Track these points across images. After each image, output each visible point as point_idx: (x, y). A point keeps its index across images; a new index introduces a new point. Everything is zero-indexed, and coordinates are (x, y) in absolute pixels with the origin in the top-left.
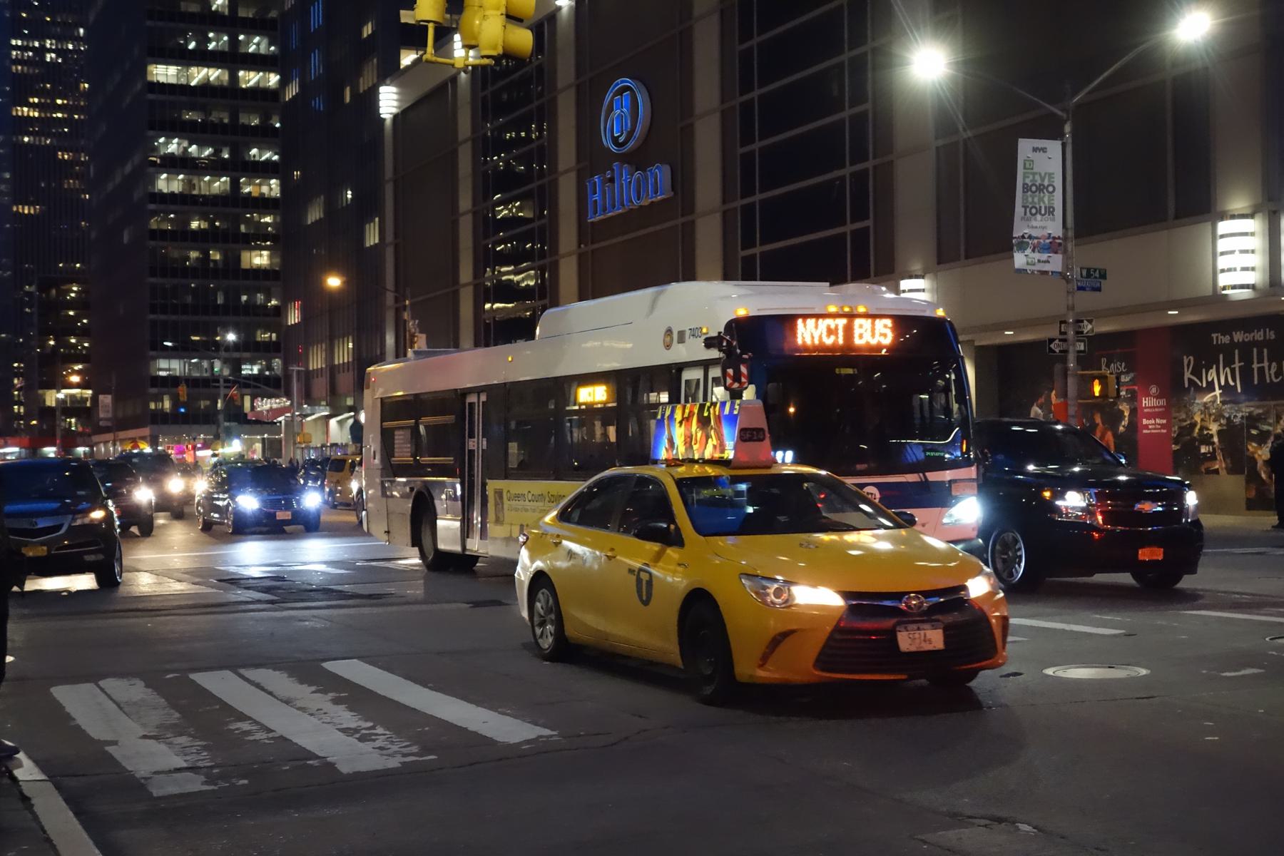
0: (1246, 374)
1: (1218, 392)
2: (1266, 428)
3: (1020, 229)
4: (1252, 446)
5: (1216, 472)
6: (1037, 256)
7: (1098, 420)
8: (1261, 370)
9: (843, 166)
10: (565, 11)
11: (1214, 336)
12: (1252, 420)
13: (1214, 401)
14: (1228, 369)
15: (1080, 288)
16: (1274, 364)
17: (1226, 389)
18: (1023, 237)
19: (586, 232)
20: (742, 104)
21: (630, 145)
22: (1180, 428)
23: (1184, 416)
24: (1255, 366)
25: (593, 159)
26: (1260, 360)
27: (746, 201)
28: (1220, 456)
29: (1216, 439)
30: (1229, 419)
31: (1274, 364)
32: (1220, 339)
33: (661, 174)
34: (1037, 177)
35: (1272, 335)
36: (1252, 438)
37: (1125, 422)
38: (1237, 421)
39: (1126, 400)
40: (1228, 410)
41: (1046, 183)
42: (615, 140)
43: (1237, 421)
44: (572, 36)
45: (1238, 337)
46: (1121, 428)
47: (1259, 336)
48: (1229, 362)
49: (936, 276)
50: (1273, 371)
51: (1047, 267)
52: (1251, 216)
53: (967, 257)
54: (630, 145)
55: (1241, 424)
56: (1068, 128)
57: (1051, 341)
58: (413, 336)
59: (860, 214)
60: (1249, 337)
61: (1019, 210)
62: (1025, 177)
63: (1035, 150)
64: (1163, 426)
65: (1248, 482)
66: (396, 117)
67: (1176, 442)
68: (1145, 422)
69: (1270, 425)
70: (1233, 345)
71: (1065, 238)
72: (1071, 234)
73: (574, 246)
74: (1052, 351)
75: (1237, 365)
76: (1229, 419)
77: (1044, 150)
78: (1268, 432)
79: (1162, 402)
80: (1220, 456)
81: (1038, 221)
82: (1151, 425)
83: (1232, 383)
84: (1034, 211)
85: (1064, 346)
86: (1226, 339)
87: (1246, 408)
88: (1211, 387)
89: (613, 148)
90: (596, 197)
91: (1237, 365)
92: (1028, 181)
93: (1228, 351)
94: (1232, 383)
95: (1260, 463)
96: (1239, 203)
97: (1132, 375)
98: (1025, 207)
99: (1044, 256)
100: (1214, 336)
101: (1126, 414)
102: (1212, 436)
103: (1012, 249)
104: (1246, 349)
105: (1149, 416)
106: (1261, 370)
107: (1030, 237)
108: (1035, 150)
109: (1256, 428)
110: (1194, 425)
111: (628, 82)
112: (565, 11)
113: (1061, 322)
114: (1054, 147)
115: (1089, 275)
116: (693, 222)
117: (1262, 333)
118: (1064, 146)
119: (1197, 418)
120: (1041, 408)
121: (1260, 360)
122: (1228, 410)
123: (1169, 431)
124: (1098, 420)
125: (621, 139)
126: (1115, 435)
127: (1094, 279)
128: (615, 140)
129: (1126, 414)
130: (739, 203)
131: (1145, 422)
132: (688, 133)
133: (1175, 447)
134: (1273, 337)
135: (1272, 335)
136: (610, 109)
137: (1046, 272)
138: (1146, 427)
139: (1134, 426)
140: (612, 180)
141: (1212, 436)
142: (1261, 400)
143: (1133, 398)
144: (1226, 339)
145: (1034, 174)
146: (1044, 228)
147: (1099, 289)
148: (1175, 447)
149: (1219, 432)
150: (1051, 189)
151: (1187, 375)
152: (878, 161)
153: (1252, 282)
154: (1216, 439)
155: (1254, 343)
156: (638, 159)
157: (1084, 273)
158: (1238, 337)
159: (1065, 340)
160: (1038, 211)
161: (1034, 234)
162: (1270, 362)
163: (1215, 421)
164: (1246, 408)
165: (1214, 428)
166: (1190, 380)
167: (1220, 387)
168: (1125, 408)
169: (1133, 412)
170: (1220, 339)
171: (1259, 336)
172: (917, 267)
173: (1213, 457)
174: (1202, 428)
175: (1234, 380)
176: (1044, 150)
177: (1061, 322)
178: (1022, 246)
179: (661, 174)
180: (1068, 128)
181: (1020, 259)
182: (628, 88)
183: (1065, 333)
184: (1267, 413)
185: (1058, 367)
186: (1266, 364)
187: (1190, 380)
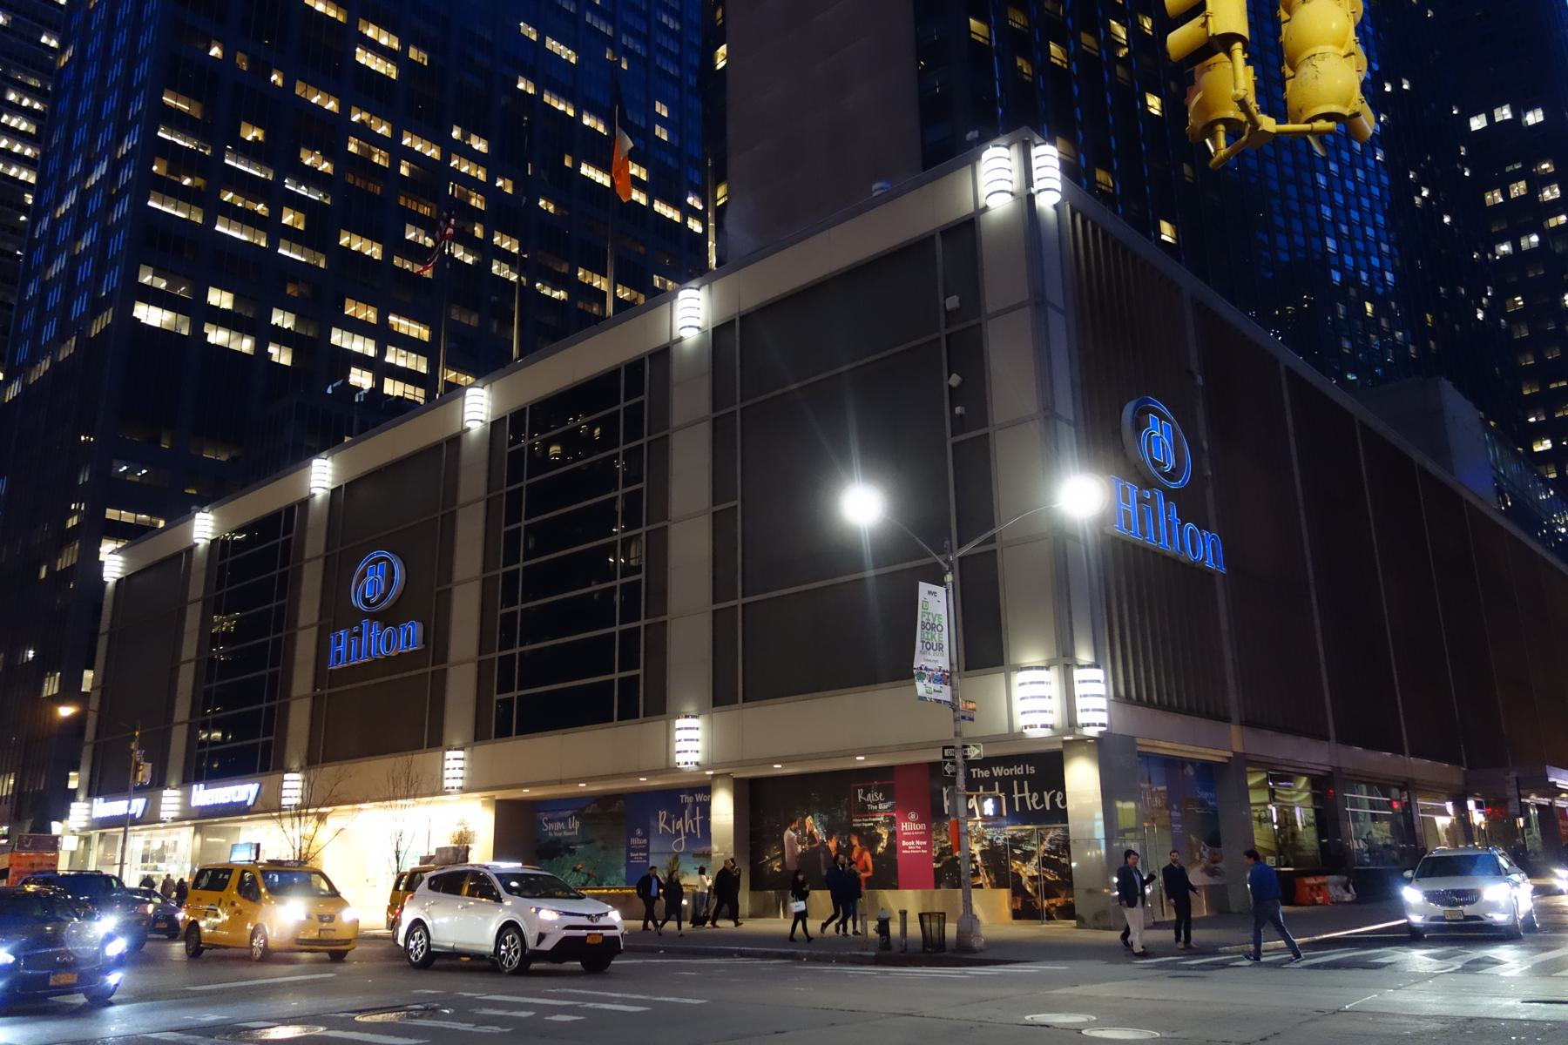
2: (1029, 848)
4: (1016, 865)
5: (980, 886)
6: (933, 686)
7: (855, 841)
8: (1022, 800)
10: (201, 547)
12: (1015, 841)
17: (689, 835)
19: (322, 676)
20: (505, 575)
21: (384, 605)
24: (1016, 796)
25: (337, 613)
26: (1021, 790)
27: (633, 625)
28: (983, 872)
29: (978, 858)
33: (415, 629)
36: (1016, 857)
37: (884, 844)
38: (1000, 842)
39: (884, 825)
40: (990, 833)
42: (366, 602)
43: (1000, 842)
44: (484, 455)
45: (998, 771)
46: (880, 849)
47: (1019, 771)
49: (711, 719)
51: (940, 697)
52: (1047, 668)
53: (744, 701)
54: (384, 605)
58: (138, 764)
59: (268, 732)
60: (1009, 772)
61: (918, 644)
64: (923, 847)
65: (1014, 895)
66: (119, 581)
67: (937, 860)
70: (992, 778)
73: (308, 689)
77: (934, 593)
78: (1033, 852)
79: (922, 826)
80: (983, 872)
81: (931, 655)
82: (910, 847)
86: (986, 774)
87: (1011, 830)
89: (364, 608)
90: (340, 648)
95: (1025, 879)
96: (1032, 657)
97: (889, 804)
99: (938, 687)
105: (908, 839)
106: (1022, 800)
111: (385, 554)
112: (201, 547)
114: (941, 590)
116: (445, 670)
121: (1021, 790)
122: (990, 833)
123: (930, 852)
124: (855, 841)
125: (373, 600)
126: (873, 856)
128: (366, 602)
132: (445, 599)
133: (935, 865)
136: (364, 575)
137: (939, 701)
138: (906, 848)
139: (892, 847)
140: (359, 634)
143: (892, 822)
144: (986, 774)
148: (935, 865)
149: (982, 853)
152: (746, 600)
153: (1049, 722)
154: (978, 858)
155: (1014, 777)
156: (390, 617)
158: (998, 771)
162: (1031, 792)
164: (1011, 830)
165: (976, 849)
168: (884, 833)
169: (892, 835)
171: (1019, 771)
172: (691, 709)
173: (976, 874)
176: (934, 593)
178: (921, 677)
179: (415, 629)
180: (949, 578)
181: (922, 688)
182: (383, 559)
186: (1027, 794)
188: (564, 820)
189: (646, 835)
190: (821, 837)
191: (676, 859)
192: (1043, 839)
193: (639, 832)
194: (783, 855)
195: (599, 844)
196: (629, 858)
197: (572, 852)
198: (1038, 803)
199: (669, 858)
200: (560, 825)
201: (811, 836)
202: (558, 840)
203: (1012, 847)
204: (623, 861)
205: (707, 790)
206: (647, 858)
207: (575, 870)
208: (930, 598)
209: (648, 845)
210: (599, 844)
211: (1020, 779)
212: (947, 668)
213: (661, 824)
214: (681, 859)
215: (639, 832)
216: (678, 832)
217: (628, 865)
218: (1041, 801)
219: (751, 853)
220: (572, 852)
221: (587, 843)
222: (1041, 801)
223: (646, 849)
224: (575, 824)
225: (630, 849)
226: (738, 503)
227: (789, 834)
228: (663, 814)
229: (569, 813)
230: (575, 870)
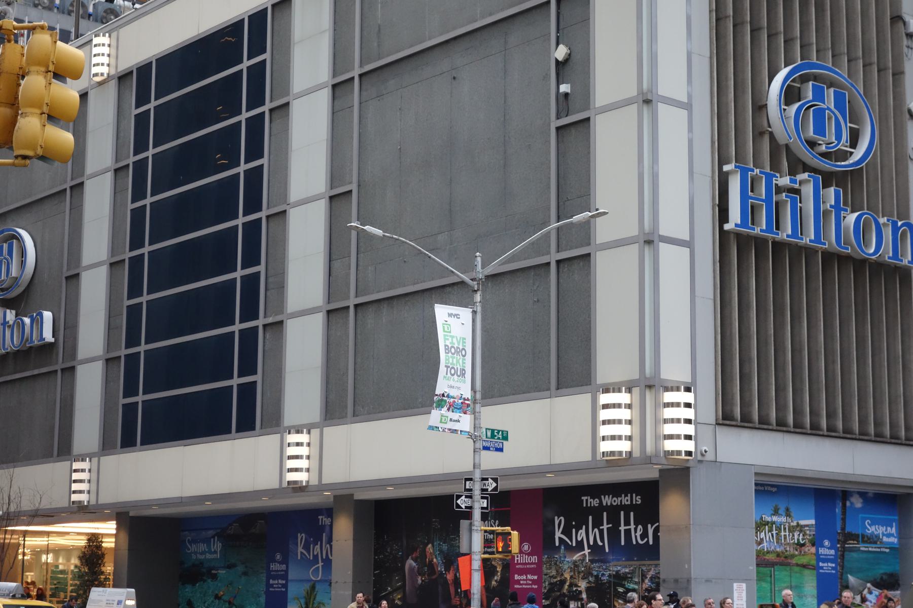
0: (614, 533)
1: (587, 551)
3: (441, 387)
8: (628, 532)
9: (233, 323)
11: (584, 498)
13: (583, 560)
14: (596, 530)
15: (486, 448)
16: (640, 527)
17: (595, 548)
18: (443, 395)
22: (550, 584)
23: (554, 573)
24: (622, 528)
26: (627, 523)
29: (584, 596)
30: (597, 577)
31: (640, 527)
32: (589, 501)
34: (455, 340)
35: (638, 500)
38: (605, 578)
41: (461, 347)
43: (605, 578)
45: (607, 500)
46: (494, 583)
47: (626, 500)
48: (598, 524)
50: (639, 533)
55: (609, 582)
56: (478, 297)
57: (459, 497)
60: (616, 501)
61: (442, 369)
62: (445, 339)
63: (450, 315)
64: (833, 568)
68: (517, 577)
69: (636, 583)
70: (602, 508)
71: (475, 401)
72: (478, 396)
74: (458, 506)
75: (605, 527)
76: (597, 577)
83: (600, 544)
84: (453, 372)
85: (469, 502)
86: (595, 503)
88: (580, 546)
91: (605, 527)
92: (448, 343)
93: (597, 513)
94: (600, 544)
98: (447, 367)
99: (455, 416)
100: (320, 517)
101: (499, 569)
102: (580, 592)
103: (431, 405)
104: (614, 512)
106: (628, 532)
107: (448, 396)
108: (450, 315)
109: (623, 586)
110: (563, 582)
113: (467, 480)
114: (465, 313)
115: (493, 436)
117: (629, 498)
118: (474, 312)
119: (567, 576)
120: (415, 561)
121: (627, 523)
122: (596, 569)
127: (496, 440)
129: (499, 569)
130: (123, 352)
131: (517, 577)
134: (639, 502)
135: (638, 500)
137: (455, 431)
138: (518, 582)
141: (580, 592)
142: (627, 560)
144: (595, 503)
145: (452, 337)
146: (459, 388)
147: (501, 450)
149: (588, 590)
150: (463, 352)
151: (558, 534)
155: (621, 507)
157: (489, 434)
158: (607, 500)
159: (470, 497)
160: (456, 372)
161: (451, 394)
162: (636, 524)
163: (583, 578)
165: (583, 585)
166: (302, 553)
167: (589, 547)
170: (589, 501)
171: (626, 500)
174: (571, 585)
175: (602, 540)
177: (467, 480)
178: (440, 405)
183: (470, 490)
184: (632, 572)
185: (464, 523)
186: (632, 527)
187: (302, 553)
188: (207, 541)
189: (285, 561)
190: (441, 568)
191: (313, 588)
192: (644, 576)
193: (278, 557)
194: (404, 585)
195: (240, 568)
196: (269, 586)
197: (214, 577)
198: (642, 537)
199: (307, 586)
200: (202, 547)
201: (431, 566)
202: (202, 563)
203: (617, 585)
204: (263, 588)
205: (329, 512)
206: (285, 586)
207: (217, 597)
208: (451, 320)
209: (286, 571)
210: (240, 568)
211: (627, 509)
212: (468, 394)
213: (300, 549)
214: (318, 587)
215: (278, 557)
216: (316, 557)
217: (268, 593)
218: (644, 535)
219: (375, 583)
220: (214, 577)
221: (230, 567)
222: (644, 535)
223: (285, 576)
224: (217, 546)
225: (269, 577)
226: (354, 187)
227: (410, 563)
228: (301, 537)
229: (211, 533)
230: (217, 597)
